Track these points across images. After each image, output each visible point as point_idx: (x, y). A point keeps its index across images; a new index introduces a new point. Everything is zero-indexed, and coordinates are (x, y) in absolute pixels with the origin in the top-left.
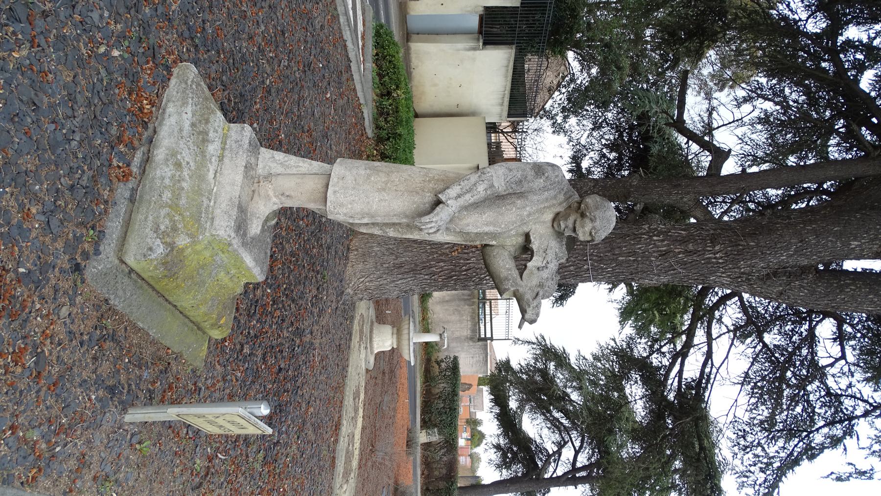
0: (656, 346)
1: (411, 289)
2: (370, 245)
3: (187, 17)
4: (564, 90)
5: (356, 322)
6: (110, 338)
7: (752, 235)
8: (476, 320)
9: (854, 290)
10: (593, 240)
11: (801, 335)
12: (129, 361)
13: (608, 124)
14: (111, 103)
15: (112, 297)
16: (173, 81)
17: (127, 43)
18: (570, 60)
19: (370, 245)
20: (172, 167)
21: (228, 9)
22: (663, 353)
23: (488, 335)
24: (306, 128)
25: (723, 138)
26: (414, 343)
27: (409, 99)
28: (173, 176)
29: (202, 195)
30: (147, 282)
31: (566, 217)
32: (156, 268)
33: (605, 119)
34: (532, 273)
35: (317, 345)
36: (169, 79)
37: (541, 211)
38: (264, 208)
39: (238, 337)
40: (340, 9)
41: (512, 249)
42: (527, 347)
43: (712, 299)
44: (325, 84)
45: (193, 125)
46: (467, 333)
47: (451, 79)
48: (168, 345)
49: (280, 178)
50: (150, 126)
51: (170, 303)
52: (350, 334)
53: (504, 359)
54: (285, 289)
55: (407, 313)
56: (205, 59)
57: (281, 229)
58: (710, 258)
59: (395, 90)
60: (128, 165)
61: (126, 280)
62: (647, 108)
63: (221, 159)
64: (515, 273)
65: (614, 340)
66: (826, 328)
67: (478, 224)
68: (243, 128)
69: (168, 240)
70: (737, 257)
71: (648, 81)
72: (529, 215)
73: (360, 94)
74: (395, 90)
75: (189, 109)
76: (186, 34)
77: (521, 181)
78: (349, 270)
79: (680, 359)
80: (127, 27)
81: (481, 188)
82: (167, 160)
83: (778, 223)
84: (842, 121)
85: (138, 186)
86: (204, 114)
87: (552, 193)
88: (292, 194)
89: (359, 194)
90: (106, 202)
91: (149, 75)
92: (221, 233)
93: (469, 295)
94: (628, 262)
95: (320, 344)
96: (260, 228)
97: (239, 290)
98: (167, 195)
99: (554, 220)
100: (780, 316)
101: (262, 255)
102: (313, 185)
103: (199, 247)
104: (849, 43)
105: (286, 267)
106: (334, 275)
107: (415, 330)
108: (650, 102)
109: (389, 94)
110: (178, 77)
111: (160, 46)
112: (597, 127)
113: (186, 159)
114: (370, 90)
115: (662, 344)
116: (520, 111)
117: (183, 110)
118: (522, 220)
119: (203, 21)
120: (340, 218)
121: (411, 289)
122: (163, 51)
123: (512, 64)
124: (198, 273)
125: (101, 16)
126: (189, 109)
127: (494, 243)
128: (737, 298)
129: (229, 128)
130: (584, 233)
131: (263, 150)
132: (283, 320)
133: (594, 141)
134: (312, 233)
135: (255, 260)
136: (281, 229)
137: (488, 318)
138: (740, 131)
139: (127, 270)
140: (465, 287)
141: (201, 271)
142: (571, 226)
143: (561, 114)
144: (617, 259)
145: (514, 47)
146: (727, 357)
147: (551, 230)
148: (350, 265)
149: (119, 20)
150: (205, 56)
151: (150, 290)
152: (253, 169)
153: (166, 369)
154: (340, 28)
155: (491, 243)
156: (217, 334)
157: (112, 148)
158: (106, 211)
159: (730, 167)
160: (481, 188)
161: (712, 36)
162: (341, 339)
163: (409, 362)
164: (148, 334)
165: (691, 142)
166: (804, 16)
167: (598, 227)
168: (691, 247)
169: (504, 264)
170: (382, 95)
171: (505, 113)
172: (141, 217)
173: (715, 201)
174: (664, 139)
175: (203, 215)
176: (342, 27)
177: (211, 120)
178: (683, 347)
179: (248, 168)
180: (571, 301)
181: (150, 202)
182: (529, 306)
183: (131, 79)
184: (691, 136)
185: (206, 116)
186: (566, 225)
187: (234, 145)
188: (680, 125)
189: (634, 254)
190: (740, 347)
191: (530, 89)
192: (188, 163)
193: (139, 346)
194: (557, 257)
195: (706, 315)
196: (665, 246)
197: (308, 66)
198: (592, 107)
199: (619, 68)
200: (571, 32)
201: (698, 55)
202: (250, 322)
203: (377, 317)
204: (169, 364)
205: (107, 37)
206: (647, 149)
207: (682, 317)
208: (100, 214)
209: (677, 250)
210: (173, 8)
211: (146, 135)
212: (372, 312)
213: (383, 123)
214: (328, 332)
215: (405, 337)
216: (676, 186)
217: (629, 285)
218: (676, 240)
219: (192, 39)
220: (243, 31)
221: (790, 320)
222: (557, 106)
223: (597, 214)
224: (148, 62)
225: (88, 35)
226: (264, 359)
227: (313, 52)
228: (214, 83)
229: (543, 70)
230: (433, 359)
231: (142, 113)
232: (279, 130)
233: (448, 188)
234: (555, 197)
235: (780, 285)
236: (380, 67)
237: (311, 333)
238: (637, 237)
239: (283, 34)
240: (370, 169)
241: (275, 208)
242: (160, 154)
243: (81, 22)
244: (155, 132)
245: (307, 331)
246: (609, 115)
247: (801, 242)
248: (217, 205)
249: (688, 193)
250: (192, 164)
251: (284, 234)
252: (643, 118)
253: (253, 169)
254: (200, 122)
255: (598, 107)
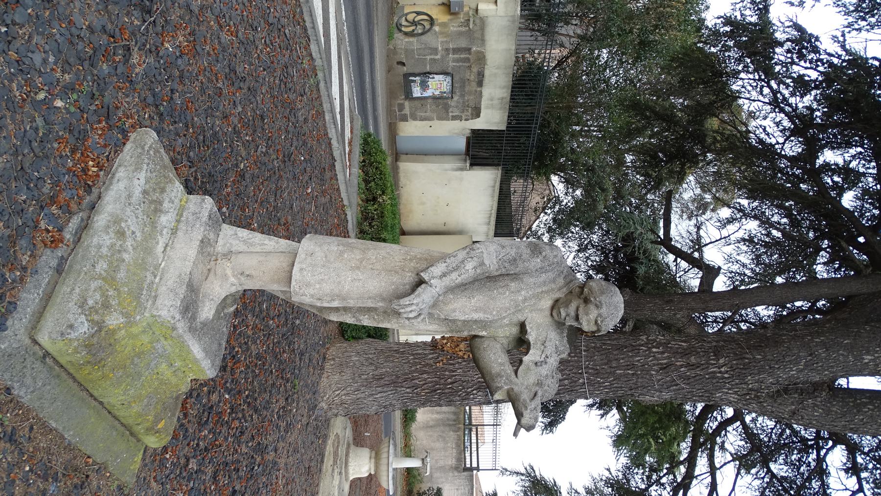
0: (654, 477)
1: (391, 404)
2: (348, 354)
3: (152, 82)
4: (549, 211)
5: (330, 442)
6: (7, 438)
7: (758, 347)
8: (462, 449)
9: (873, 410)
10: (599, 330)
11: (809, 466)
12: (31, 470)
13: (592, 245)
14: (47, 157)
15: (16, 385)
16: (128, 146)
17: (75, 96)
18: (555, 183)
19: (348, 354)
20: (113, 235)
21: (202, 83)
22: (663, 485)
23: (475, 465)
24: (283, 221)
25: (712, 255)
26: (395, 470)
27: (396, 214)
28: (112, 245)
29: (146, 270)
30: (66, 370)
31: (567, 304)
32: (76, 351)
33: (590, 241)
34: (528, 369)
35: (282, 465)
36: (124, 144)
37: (538, 297)
38: (220, 288)
39: (183, 448)
40: (326, 106)
41: (505, 342)
42: (515, 478)
43: (711, 424)
44: (307, 178)
45: (145, 192)
46: (452, 462)
47: (438, 198)
48: (88, 453)
49: (240, 256)
50: (95, 191)
51: (95, 399)
52: (322, 455)
53: (491, 492)
54: (247, 397)
55: (387, 434)
56: (170, 131)
57: (247, 327)
58: (714, 372)
59: (380, 195)
60: (60, 230)
61: (38, 365)
62: (632, 230)
63: (174, 231)
64: (509, 369)
65: (608, 470)
66: (837, 457)
67: (467, 309)
68: (204, 200)
69: (96, 318)
70: (744, 372)
71: (631, 204)
72: (525, 300)
73: (344, 195)
74: (380, 195)
75: (142, 175)
76: (150, 100)
77: (515, 260)
78: (324, 381)
79: (682, 491)
80: (78, 80)
81: (470, 266)
82: (108, 227)
83: (785, 335)
84: (826, 242)
85: (70, 254)
86: (160, 182)
87: (551, 275)
88: (253, 273)
89: (330, 274)
90: (24, 269)
91: (100, 135)
92: (164, 313)
93: (454, 421)
94: (626, 375)
95: (286, 464)
96: (213, 312)
97: (185, 388)
98: (102, 266)
99: (553, 308)
100: (785, 444)
101: (215, 347)
102: (277, 263)
103: (135, 330)
104: (826, 166)
105: (250, 371)
106: (307, 386)
107: (396, 455)
108: (634, 223)
109: (374, 199)
110: (134, 142)
111: (117, 108)
112: (582, 249)
113: (132, 228)
114: (355, 195)
115: (662, 475)
116: (506, 231)
117: (135, 174)
118: (517, 306)
119: (172, 91)
120: (307, 300)
121: (391, 404)
122: (120, 114)
123: (498, 184)
124: (132, 363)
125: (45, 61)
126: (142, 175)
127: (484, 333)
128: (738, 423)
129: (187, 199)
130: (588, 321)
131: (225, 226)
132: (242, 433)
133: (580, 262)
134: (283, 335)
135: (205, 350)
136: (247, 327)
137: (474, 446)
138: (729, 249)
139: (41, 353)
140: (450, 403)
141: (136, 360)
142: (573, 314)
143: (547, 235)
144: (614, 372)
145: (500, 168)
146: (733, 489)
147: (549, 319)
148: (325, 375)
149: (68, 69)
150: (171, 127)
151: (70, 381)
152: (211, 246)
153: (83, 483)
154: (324, 125)
155: (481, 334)
156: (154, 442)
157: (42, 208)
158: (22, 279)
159: (720, 285)
160: (470, 266)
161: (693, 157)
162: (311, 460)
163: (388, 491)
164: (62, 437)
165: (679, 260)
166: (781, 140)
167: (605, 314)
168: (693, 360)
169: (496, 358)
170: (367, 201)
171: (492, 233)
172: (66, 289)
173: (707, 321)
174: (650, 260)
175: (144, 292)
176: (328, 125)
177: (168, 189)
178: (683, 479)
179: (204, 243)
180: (561, 427)
181: (79, 273)
182: (526, 408)
183: (77, 135)
184: (679, 254)
185: (162, 185)
186: (567, 313)
187: (191, 218)
188: (667, 243)
189: (632, 366)
190: (746, 479)
191: (517, 210)
192: (133, 233)
193: (48, 451)
194: (557, 351)
195: (706, 442)
196: (665, 358)
197: (288, 157)
198: (577, 229)
199: (603, 190)
200: (556, 154)
201: (681, 179)
202: (200, 431)
203: (354, 439)
204: (87, 476)
205: (50, 85)
206: (633, 270)
207: (678, 445)
208: (14, 281)
209: (678, 364)
210: (137, 70)
211: (88, 199)
212: (349, 433)
213: (367, 228)
214: (296, 451)
215: (384, 461)
216: (668, 302)
217: (620, 409)
218: (677, 352)
219: (157, 106)
220: (217, 108)
221: (796, 448)
222: (542, 226)
223: (603, 298)
224: (100, 122)
225: (25, 77)
226: (215, 478)
227: (295, 143)
228: (179, 157)
229: (530, 193)
230: (415, 491)
231: (86, 175)
232: (252, 218)
233: (432, 266)
234: (554, 281)
235: (792, 404)
236: (366, 173)
237: (276, 451)
238: (635, 349)
239: (262, 118)
240: (343, 244)
241: (233, 290)
242: (101, 220)
243: (17, 61)
244: (100, 197)
245: (270, 448)
246: (595, 237)
247: (811, 355)
248: (162, 282)
249: (681, 309)
250: (138, 234)
251: (250, 333)
252: (628, 239)
253: (211, 246)
254: (154, 190)
255: (583, 229)
